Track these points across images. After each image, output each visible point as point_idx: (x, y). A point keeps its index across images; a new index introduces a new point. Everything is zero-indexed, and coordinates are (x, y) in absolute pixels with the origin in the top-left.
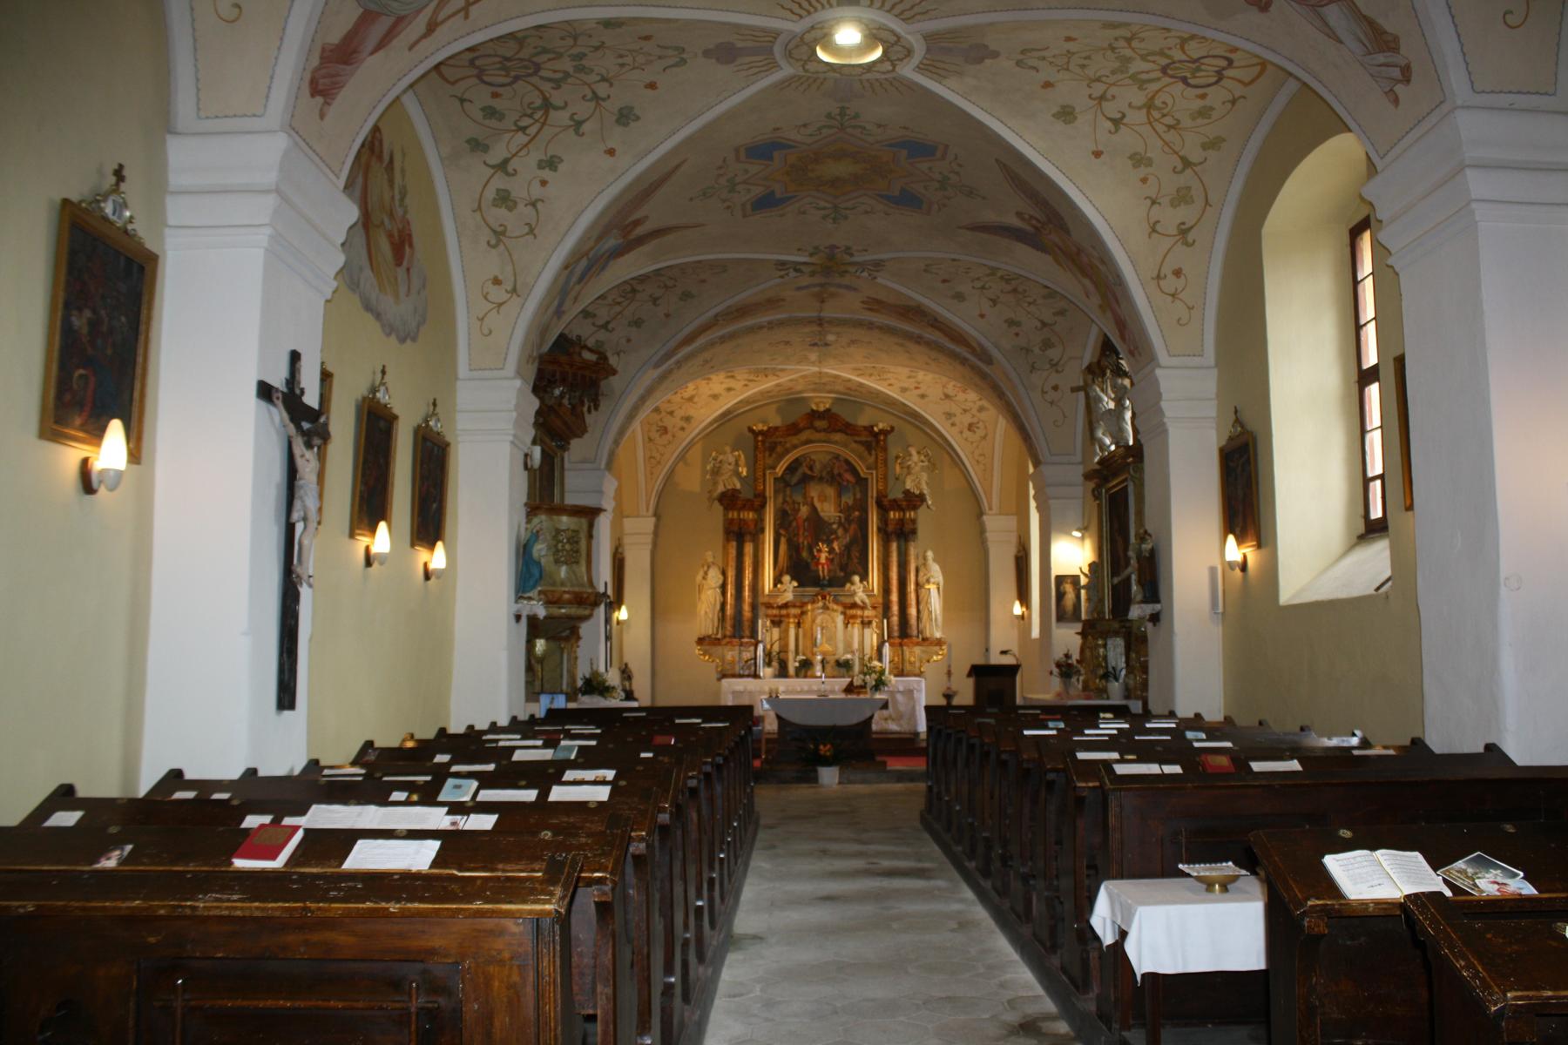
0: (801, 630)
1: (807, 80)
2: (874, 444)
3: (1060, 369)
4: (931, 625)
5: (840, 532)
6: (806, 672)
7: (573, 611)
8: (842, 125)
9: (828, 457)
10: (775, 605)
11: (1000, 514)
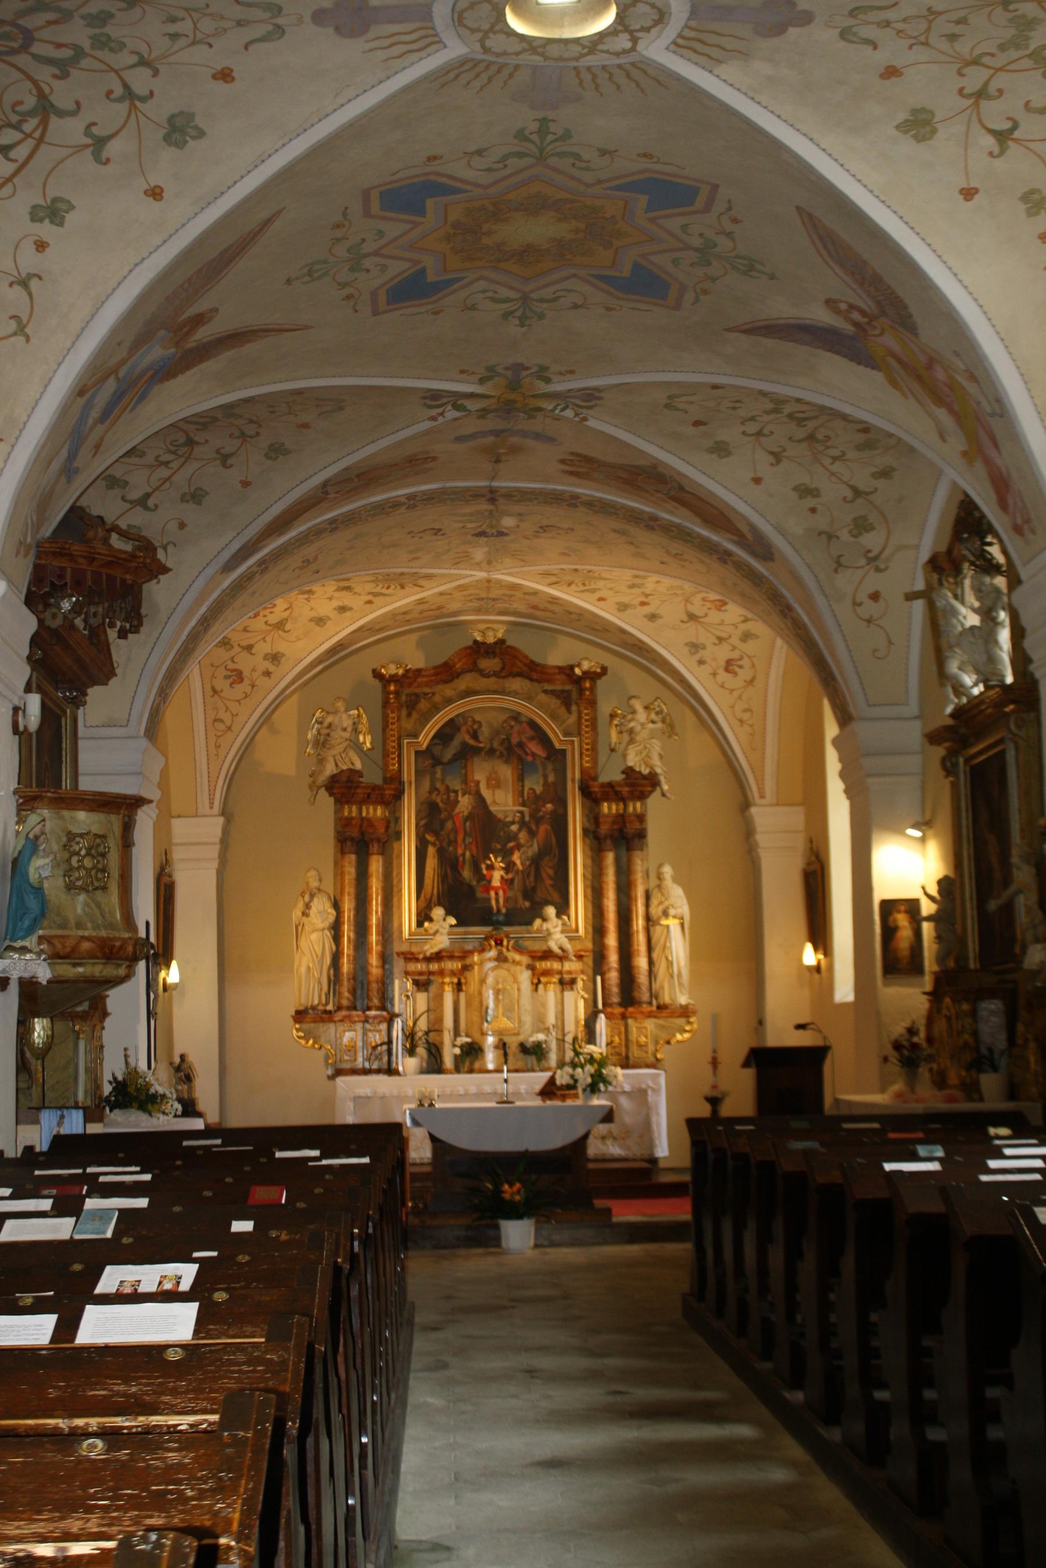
0: (462, 996)
1: (487, 68)
2: (574, 695)
3: (882, 566)
4: (672, 986)
5: (523, 836)
6: (472, 1063)
7: (97, 970)
8: (541, 150)
9: (503, 717)
10: (421, 956)
11: (777, 804)
